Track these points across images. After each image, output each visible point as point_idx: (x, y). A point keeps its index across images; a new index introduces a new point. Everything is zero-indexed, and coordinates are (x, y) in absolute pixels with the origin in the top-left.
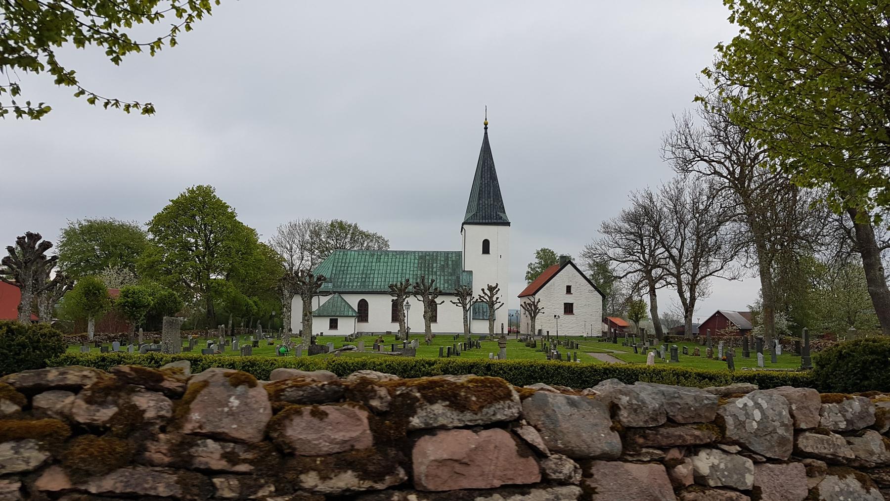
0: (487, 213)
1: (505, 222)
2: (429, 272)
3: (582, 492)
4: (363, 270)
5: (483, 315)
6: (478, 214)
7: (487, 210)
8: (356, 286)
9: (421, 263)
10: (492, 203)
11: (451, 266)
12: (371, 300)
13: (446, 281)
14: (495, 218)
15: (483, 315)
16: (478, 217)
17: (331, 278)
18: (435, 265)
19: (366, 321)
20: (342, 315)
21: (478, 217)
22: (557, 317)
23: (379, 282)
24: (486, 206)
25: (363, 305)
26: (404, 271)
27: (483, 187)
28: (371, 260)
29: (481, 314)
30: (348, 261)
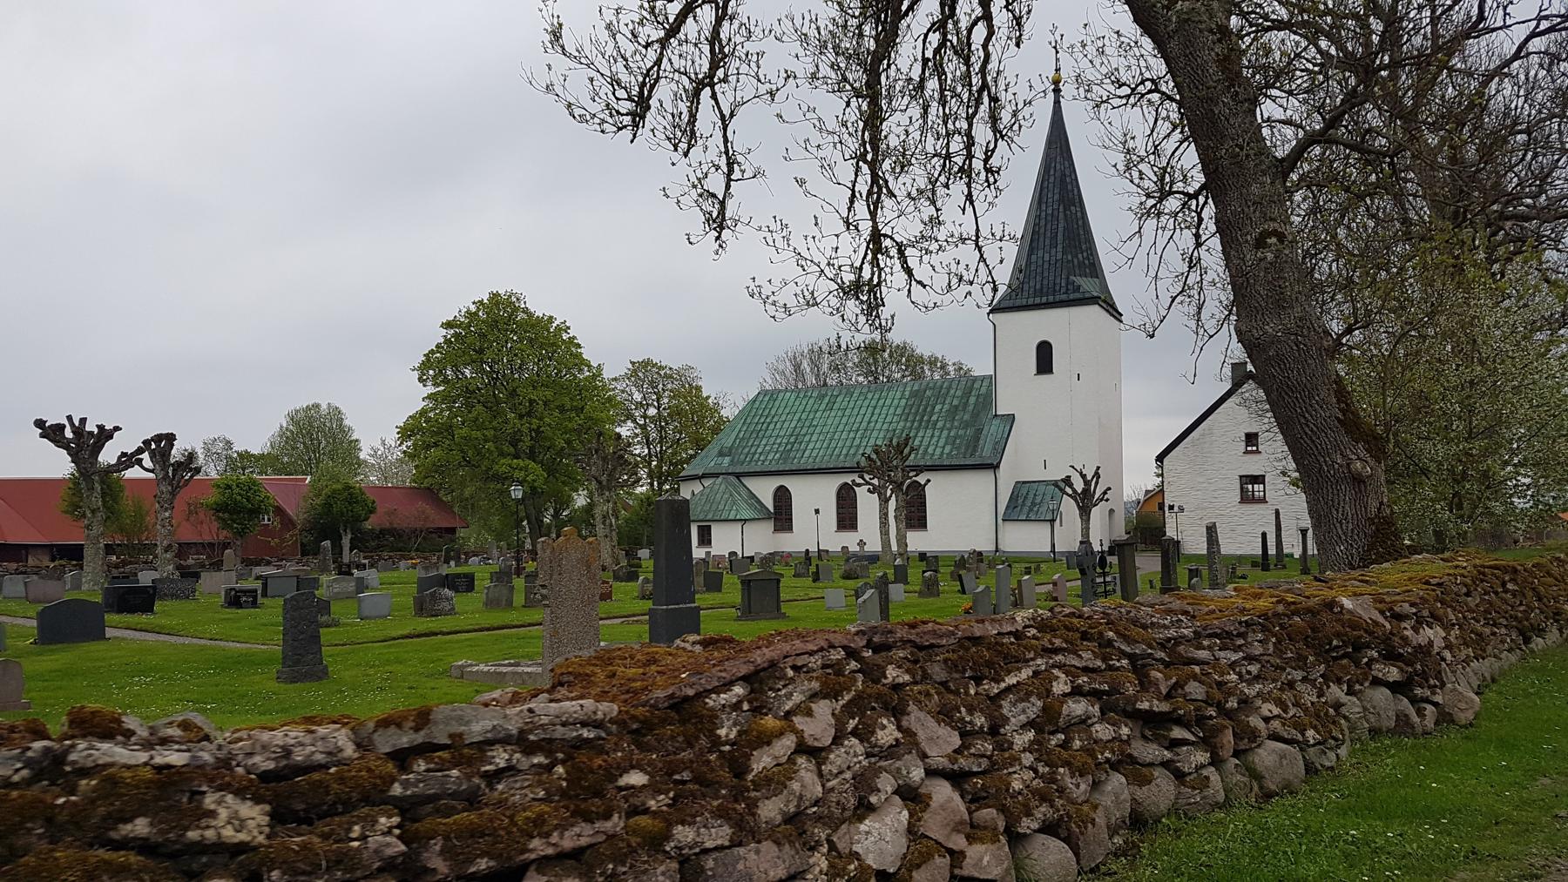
0: (1045, 282)
1: (1087, 295)
2: (920, 424)
3: (267, 808)
4: (795, 427)
5: (1031, 510)
6: (1026, 287)
7: (1046, 274)
8: (772, 460)
9: (912, 406)
10: (1059, 256)
11: (971, 408)
12: (794, 485)
13: (950, 441)
14: (1063, 290)
15: (1031, 510)
16: (1026, 294)
17: (731, 449)
18: (938, 407)
19: (790, 529)
20: (718, 518)
21: (1026, 294)
22: (1176, 509)
23: (814, 451)
24: (1046, 266)
25: (782, 496)
26: (872, 424)
27: (1042, 223)
28: (816, 406)
29: (1026, 509)
30: (773, 412)
